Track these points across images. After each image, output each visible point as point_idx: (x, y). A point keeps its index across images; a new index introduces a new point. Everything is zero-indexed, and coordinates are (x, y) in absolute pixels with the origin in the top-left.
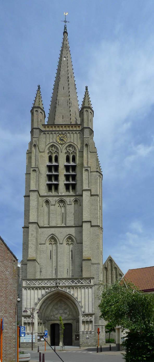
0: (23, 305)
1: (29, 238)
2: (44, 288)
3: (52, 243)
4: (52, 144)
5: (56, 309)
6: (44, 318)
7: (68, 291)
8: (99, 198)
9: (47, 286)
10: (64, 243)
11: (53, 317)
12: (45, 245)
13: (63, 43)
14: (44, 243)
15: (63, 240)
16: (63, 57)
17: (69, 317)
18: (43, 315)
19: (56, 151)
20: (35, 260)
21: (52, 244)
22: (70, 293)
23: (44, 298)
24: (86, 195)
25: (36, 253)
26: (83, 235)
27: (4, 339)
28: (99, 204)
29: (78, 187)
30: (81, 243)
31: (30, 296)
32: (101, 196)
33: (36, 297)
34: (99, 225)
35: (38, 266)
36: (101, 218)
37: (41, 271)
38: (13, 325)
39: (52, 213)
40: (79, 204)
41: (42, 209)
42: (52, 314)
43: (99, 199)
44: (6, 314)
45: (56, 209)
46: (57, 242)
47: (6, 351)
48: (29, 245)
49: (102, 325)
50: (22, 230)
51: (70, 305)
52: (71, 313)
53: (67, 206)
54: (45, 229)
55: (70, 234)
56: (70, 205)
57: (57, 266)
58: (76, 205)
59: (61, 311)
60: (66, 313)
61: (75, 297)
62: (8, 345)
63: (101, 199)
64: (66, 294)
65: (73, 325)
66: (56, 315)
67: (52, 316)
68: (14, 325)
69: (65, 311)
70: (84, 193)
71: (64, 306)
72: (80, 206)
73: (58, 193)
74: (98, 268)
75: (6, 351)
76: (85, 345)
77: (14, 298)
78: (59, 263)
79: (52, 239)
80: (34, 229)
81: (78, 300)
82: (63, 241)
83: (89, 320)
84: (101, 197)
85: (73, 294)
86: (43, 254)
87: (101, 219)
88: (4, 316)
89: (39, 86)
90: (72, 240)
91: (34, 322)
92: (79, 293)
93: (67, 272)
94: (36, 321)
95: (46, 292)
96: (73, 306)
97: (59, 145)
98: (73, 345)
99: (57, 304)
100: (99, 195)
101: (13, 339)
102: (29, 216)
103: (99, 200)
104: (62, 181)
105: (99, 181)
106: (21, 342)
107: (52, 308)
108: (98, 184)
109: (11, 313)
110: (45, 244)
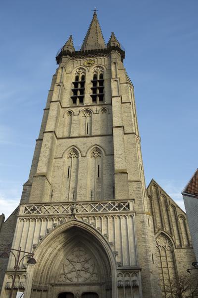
2: (51, 218)
8: (131, 106)
9: (58, 215)
12: (62, 160)
14: (61, 156)
15: (88, 151)
17: (92, 279)
20: (44, 176)
22: (95, 226)
24: (115, 102)
25: (48, 168)
28: (132, 112)
30: (111, 155)
31: (27, 233)
32: (133, 102)
33: (37, 235)
34: (134, 132)
37: (52, 195)
43: (131, 107)
45: (80, 119)
46: (78, 156)
52: (96, 271)
53: (93, 115)
57: (76, 187)
58: (104, 114)
59: (78, 266)
60: (86, 270)
61: (103, 234)
66: (69, 273)
67: (63, 276)
69: (87, 266)
71: (85, 255)
72: (109, 114)
80: (49, 139)
81: (109, 239)
83: (131, 284)
84: (133, 104)
87: (136, 127)
90: (100, 152)
93: (92, 195)
95: (54, 226)
96: (100, 255)
103: (131, 108)
104: (88, 93)
105: (130, 91)
108: (130, 94)
110: (62, 158)
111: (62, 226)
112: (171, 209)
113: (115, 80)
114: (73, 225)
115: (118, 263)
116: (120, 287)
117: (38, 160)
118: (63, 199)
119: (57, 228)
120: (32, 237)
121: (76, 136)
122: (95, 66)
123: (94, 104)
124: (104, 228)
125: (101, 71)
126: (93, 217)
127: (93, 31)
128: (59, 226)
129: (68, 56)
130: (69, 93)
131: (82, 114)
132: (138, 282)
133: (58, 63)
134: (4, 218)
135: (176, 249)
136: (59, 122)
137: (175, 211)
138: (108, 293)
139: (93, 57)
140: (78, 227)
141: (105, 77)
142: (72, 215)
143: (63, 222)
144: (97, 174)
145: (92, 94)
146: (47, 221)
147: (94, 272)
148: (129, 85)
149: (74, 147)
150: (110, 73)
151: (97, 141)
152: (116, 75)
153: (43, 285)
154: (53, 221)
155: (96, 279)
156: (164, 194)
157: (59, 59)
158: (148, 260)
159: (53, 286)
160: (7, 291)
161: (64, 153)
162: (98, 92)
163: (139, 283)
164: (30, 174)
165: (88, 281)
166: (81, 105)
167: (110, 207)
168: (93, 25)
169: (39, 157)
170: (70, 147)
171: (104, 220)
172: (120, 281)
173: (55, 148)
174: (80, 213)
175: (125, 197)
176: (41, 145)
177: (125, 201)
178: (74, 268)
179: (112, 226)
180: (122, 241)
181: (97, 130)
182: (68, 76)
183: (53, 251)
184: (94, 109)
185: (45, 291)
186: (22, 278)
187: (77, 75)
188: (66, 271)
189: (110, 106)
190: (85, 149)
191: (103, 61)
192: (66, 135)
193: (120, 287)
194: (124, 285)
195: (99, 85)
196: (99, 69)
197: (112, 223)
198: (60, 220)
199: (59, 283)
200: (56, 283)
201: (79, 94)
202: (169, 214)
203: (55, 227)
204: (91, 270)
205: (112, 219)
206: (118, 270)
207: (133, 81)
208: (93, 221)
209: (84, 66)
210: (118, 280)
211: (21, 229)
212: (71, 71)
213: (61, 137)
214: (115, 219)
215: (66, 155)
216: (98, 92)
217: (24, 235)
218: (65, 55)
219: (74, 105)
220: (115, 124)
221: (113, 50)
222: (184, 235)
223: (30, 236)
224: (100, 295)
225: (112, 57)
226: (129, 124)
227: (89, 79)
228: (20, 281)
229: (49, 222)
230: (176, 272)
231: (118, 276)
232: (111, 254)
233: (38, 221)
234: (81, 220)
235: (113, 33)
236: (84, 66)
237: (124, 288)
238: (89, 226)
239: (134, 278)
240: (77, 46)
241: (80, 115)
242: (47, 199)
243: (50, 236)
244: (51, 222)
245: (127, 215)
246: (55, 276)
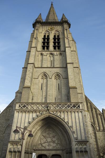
0: (13, 121)
2: (35, 111)
6: (31, 147)
7: (59, 114)
9: (39, 110)
10: (52, 78)
12: (38, 79)
14: (37, 78)
17: (57, 147)
22: (61, 117)
25: (31, 84)
33: (27, 121)
35: (31, 94)
37: (33, 99)
41: (38, 57)
46: (47, 78)
50: (22, 69)
52: (59, 143)
55: (58, 72)
57: (46, 95)
59: (49, 140)
60: (54, 142)
64: (57, 118)
66: (44, 143)
67: (40, 145)
69: (54, 139)
71: (53, 133)
74: (82, 97)
78: (48, 93)
82: (52, 77)
83: (83, 150)
90: (59, 77)
92: (70, 117)
93: (55, 100)
95: (37, 116)
104: (51, 44)
105: (74, 45)
106: (55, 102)
108: (74, 46)
110: (38, 78)
111: (42, 116)
112: (94, 110)
113: (67, 39)
114: (48, 116)
115: (75, 138)
116: (77, 152)
117: (25, 79)
118: (39, 101)
119: (39, 117)
120: (24, 122)
121: (45, 67)
122: (55, 30)
123: (55, 50)
124: (66, 118)
125: (48, 33)
126: (60, 112)
127: (51, 13)
128: (40, 116)
129: (40, 24)
130: (41, 44)
131: (48, 56)
132: (87, 149)
133: (34, 27)
135: (97, 131)
136: (35, 58)
137: (96, 111)
138: (67, 155)
139: (53, 25)
140: (51, 117)
141: (61, 37)
142: (47, 110)
143: (43, 114)
144: (58, 88)
145: (42, 45)
146: (33, 113)
147: (58, 143)
148: (74, 42)
149: (45, 73)
150: (64, 35)
151: (58, 70)
152: (67, 36)
153: (29, 150)
154: (36, 113)
155: (60, 147)
156: (90, 102)
157: (34, 25)
158: (89, 137)
159: (35, 151)
160: (10, 153)
161: (39, 76)
162: (57, 44)
163: (87, 149)
164: (20, 86)
165: (55, 148)
166: (47, 50)
167: (69, 106)
168: (51, 9)
169: (25, 77)
170: (42, 73)
171: (66, 113)
172: (77, 148)
173: (34, 73)
174: (52, 109)
175: (76, 102)
176: (26, 71)
177: (77, 103)
178: (47, 140)
179: (71, 117)
180: (77, 125)
181: (57, 64)
182: (40, 35)
183: (35, 131)
184: (55, 53)
185: (30, 153)
186: (19, 146)
187: (45, 34)
188: (42, 142)
189: (64, 53)
191: (59, 28)
192: (40, 66)
193: (77, 152)
194: (79, 150)
195: (57, 41)
196: (57, 32)
197: (71, 115)
198: (41, 112)
199: (38, 149)
200: (37, 149)
201: (46, 44)
202: (93, 113)
203: (37, 117)
204: (56, 142)
205: (70, 113)
206: (75, 142)
207: (75, 40)
208: (59, 114)
209: (49, 30)
210: (76, 147)
211: (17, 117)
212: (42, 32)
213: (37, 67)
214: (72, 113)
215: (40, 77)
216: (57, 44)
217: (19, 120)
218: (66, 23)
219: (44, 50)
220: (68, 62)
221: (64, 22)
222: (101, 124)
223: (23, 122)
224: (62, 156)
225: (64, 27)
227: (51, 37)
228: (18, 147)
229: (34, 114)
230: (97, 144)
231: (76, 145)
232: (71, 133)
233: (27, 113)
234: (53, 113)
235: (40, 14)
236: (49, 30)
237: (84, 152)
238: (58, 117)
239: (85, 146)
240: (44, 19)
241: (47, 55)
242: (30, 101)
243: (35, 122)
244: (35, 114)
245: (79, 111)
246: (36, 145)
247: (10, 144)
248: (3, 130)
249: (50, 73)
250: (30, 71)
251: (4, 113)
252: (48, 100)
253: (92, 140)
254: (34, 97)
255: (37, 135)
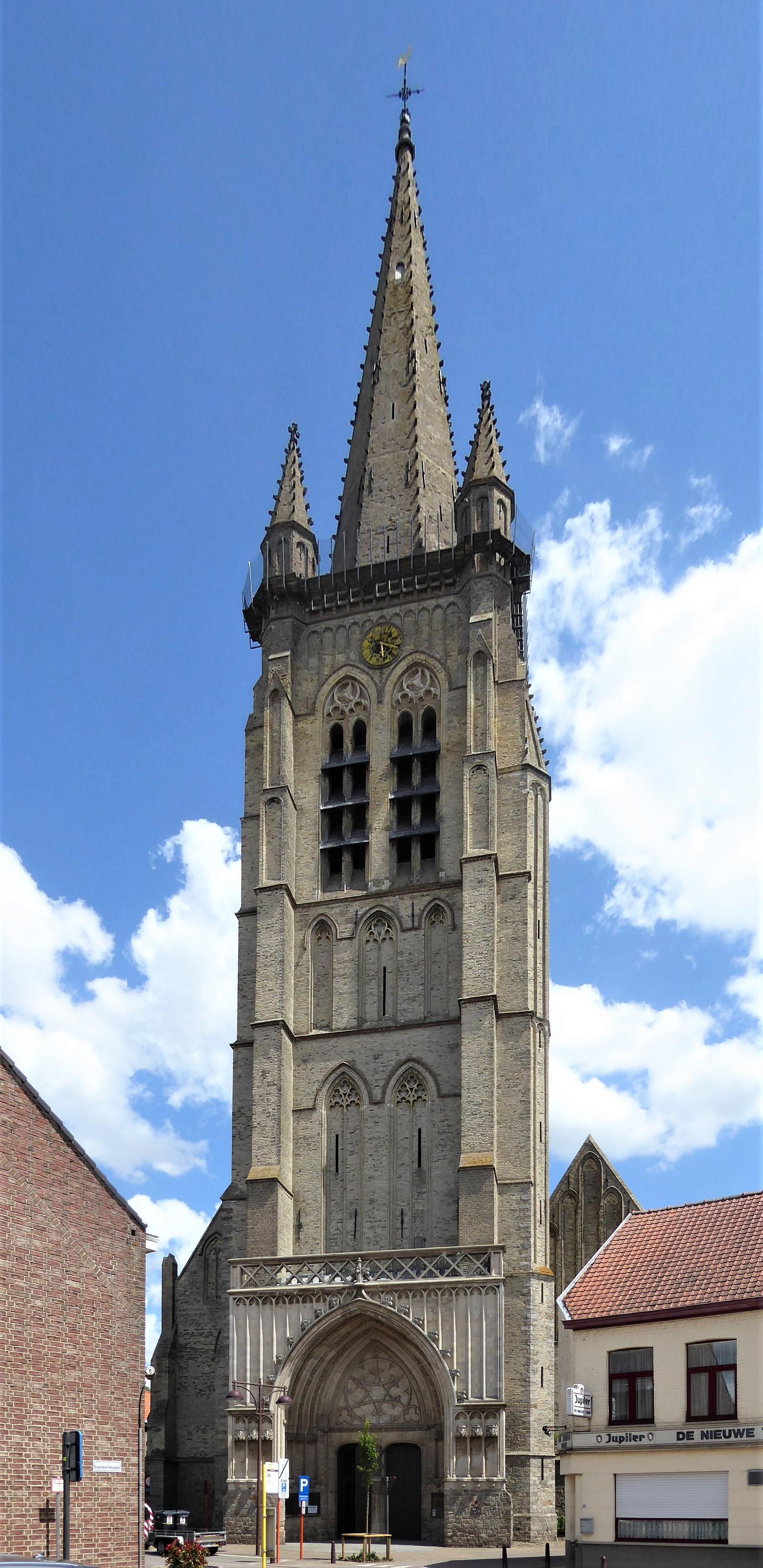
1: (255, 1091)
3: (340, 1101)
4: (342, 673)
5: (359, 1382)
6: (311, 1422)
8: (530, 885)
10: (387, 1097)
11: (345, 1416)
13: (393, 200)
14: (310, 1104)
16: (393, 264)
17: (408, 1417)
18: (307, 1407)
19: (358, 704)
21: (342, 1106)
23: (307, 1336)
26: (463, 1061)
27: (99, 1515)
28: (530, 911)
29: (445, 848)
32: (540, 874)
34: (531, 1009)
36: (540, 974)
38: (130, 1465)
39: (340, 976)
40: (450, 923)
42: (342, 1403)
44: (107, 1423)
47: (105, 1555)
48: (256, 1120)
49: (542, 1454)
50: (236, 921)
51: (411, 1365)
52: (415, 1401)
54: (314, 1044)
55: (415, 1056)
56: (414, 932)
60: (395, 1400)
62: (113, 1534)
63: (540, 890)
65: (423, 1449)
66: (359, 1407)
67: (345, 1414)
68: (133, 1465)
69: (395, 1391)
70: (468, 869)
73: (366, 888)
75: (105, 1555)
76: (468, 1540)
77: (134, 1366)
79: (342, 1086)
84: (540, 883)
85: (419, 1321)
86: (305, 1153)
87: (540, 980)
88: (99, 1433)
89: (296, 429)
91: (272, 1438)
94: (279, 1435)
97: (371, 672)
98: (423, 1536)
99: (360, 1362)
100: (532, 875)
101: (130, 1514)
102: (254, 998)
107: (343, 1376)
109: (122, 1419)
133: (255, 635)
134: (175, 1265)
170: (334, 1071)
185: (309, 1442)
188: (351, 1403)
190: (377, 1077)
199: (338, 1427)
226: (517, 973)
247: (235, 1419)
248: (207, 1347)
249: (372, 1066)
250: (270, 1079)
251: (195, 1273)
252: (368, 1225)
253: (544, 1392)
254: (303, 1214)
255: (330, 1378)
